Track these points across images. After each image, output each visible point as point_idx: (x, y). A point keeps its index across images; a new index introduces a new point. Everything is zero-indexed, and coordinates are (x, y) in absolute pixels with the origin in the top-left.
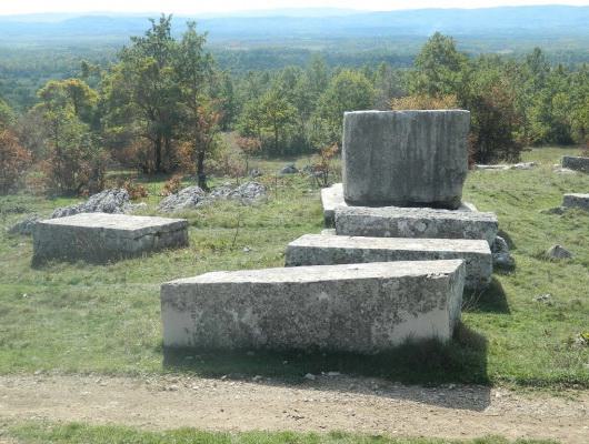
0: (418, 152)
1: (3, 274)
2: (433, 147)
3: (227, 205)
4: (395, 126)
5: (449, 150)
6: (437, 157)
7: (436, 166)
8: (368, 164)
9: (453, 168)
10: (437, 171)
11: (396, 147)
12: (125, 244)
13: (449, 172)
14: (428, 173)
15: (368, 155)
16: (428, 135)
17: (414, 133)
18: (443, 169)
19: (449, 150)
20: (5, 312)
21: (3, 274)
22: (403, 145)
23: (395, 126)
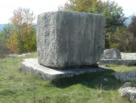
0: (88, 37)
1: (58, 102)
2: (94, 34)
3: (102, 34)
4: (80, 20)
5: (99, 36)
6: (95, 39)
7: (95, 44)
8: (68, 44)
9: (100, 46)
10: (95, 47)
11: (80, 33)
12: (77, 64)
13: (99, 47)
14: (92, 48)
15: (67, 38)
16: (92, 27)
17: (87, 25)
18: (97, 46)
19: (99, 36)
20: (1, 87)
21: (58, 102)
22: (83, 33)
23: (80, 20)
